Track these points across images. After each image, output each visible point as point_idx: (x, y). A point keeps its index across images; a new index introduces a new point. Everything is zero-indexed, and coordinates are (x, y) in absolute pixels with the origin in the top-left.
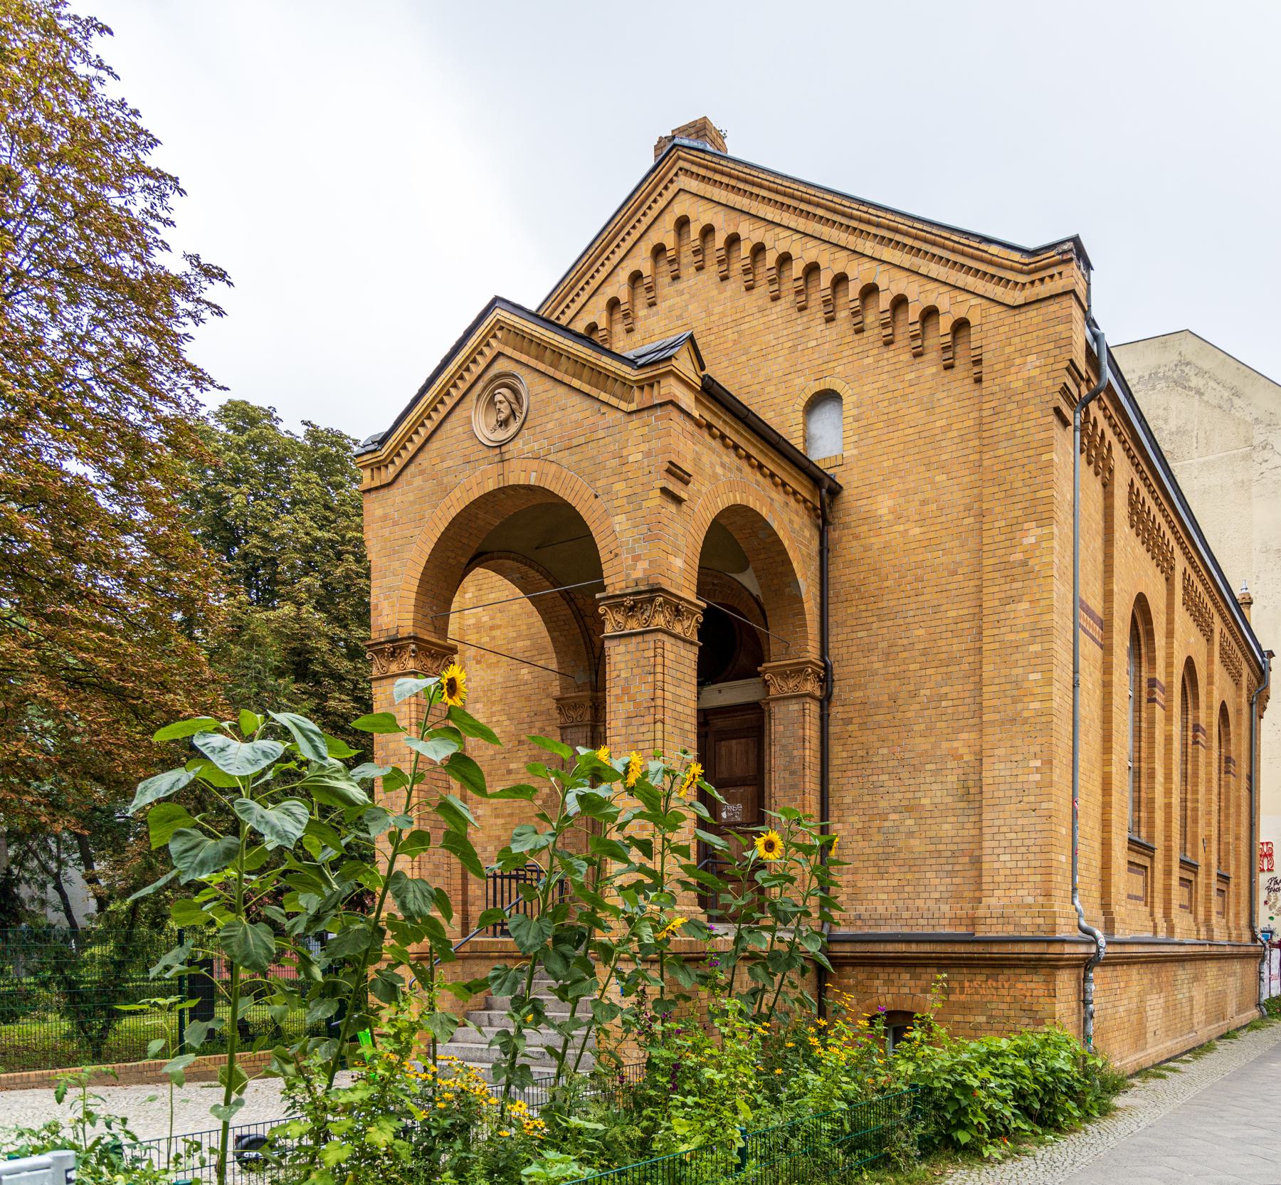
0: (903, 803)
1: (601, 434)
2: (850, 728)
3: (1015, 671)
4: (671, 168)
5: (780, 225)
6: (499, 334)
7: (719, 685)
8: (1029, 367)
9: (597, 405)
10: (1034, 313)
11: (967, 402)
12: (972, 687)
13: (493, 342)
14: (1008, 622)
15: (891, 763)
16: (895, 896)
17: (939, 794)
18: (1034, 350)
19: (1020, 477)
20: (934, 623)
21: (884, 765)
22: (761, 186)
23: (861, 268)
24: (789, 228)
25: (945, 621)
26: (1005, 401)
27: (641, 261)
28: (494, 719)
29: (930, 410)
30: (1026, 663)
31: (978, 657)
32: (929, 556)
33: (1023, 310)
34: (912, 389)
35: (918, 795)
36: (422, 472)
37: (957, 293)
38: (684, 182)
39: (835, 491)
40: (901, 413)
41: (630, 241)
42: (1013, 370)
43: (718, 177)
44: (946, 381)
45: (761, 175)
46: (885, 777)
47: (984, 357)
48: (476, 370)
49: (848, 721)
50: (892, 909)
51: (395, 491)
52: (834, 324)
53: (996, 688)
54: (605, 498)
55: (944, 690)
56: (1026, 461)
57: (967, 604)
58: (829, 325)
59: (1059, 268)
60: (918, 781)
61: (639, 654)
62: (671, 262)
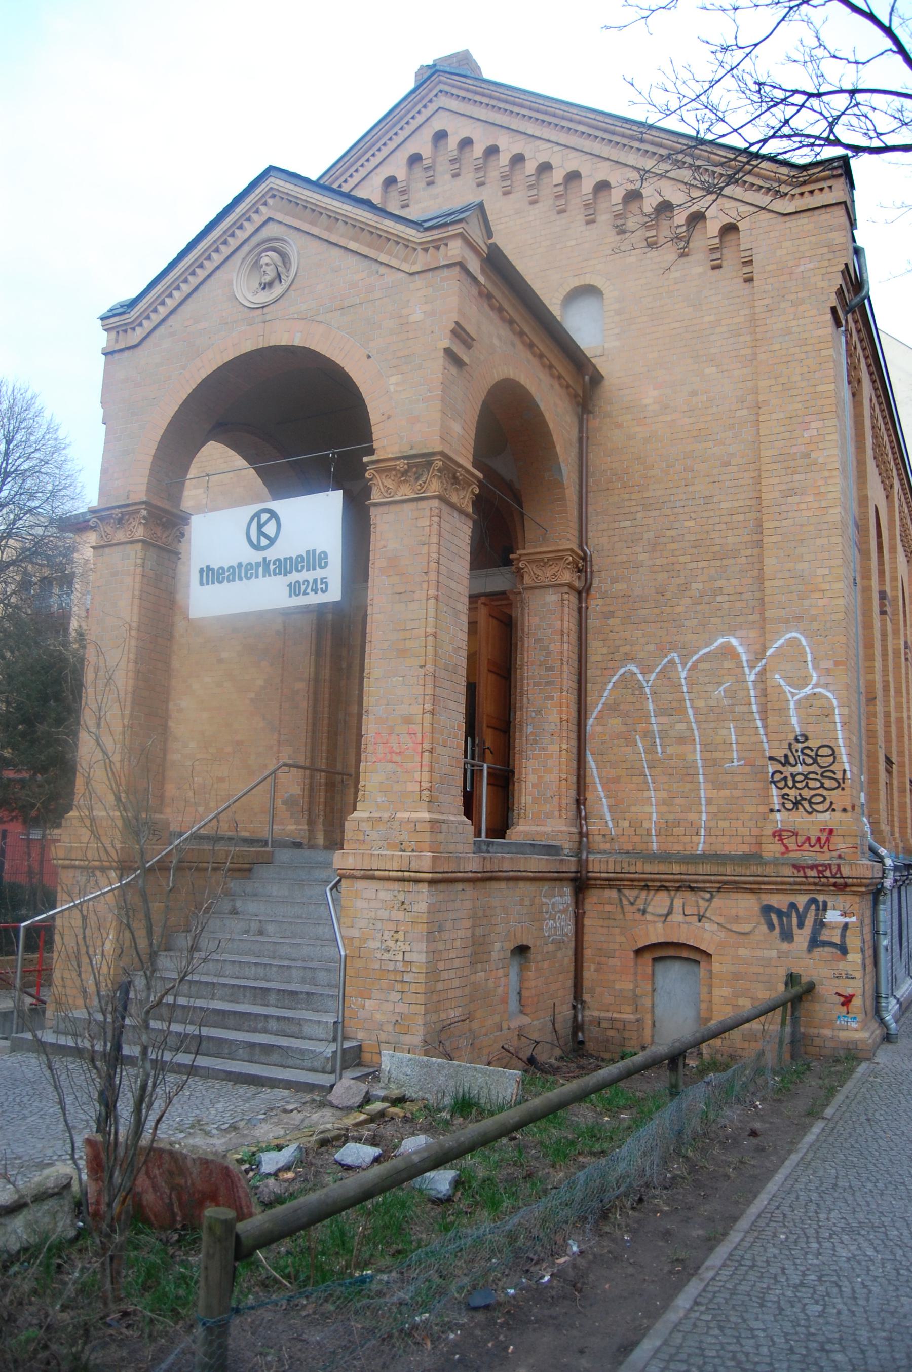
2: (611, 621)
5: (541, 139)
6: (271, 201)
9: (375, 266)
10: (806, 221)
12: (750, 581)
13: (263, 209)
14: (790, 515)
20: (705, 514)
22: (521, 106)
24: (549, 141)
27: (397, 168)
31: (756, 551)
38: (444, 101)
39: (597, 379)
41: (385, 151)
43: (478, 98)
45: (522, 96)
47: (754, 258)
48: (241, 235)
49: (610, 615)
51: (138, 351)
52: (594, 225)
56: (803, 356)
58: (589, 227)
59: (829, 183)
62: (427, 169)
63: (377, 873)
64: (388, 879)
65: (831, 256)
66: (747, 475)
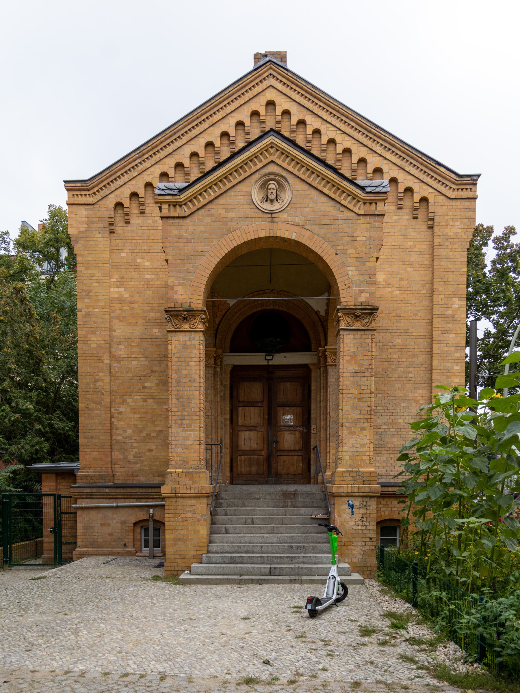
0: (389, 421)
1: (340, 222)
3: (448, 365)
4: (265, 72)
5: (330, 123)
7: (285, 354)
8: (456, 227)
10: (459, 204)
11: (423, 237)
14: (445, 342)
15: (383, 401)
16: (385, 465)
17: (407, 417)
18: (459, 220)
19: (452, 276)
20: (406, 337)
21: (380, 402)
23: (374, 158)
24: (335, 126)
25: (411, 337)
26: (445, 240)
28: (133, 356)
29: (405, 236)
30: (453, 361)
32: (404, 305)
33: (454, 201)
34: (396, 224)
35: (397, 417)
36: (211, 216)
37: (422, 184)
38: (272, 81)
40: (390, 234)
42: (449, 227)
44: (413, 224)
46: (380, 408)
47: (435, 217)
50: (384, 471)
51: (188, 221)
53: (439, 371)
54: (342, 256)
55: (411, 369)
56: (454, 270)
57: (422, 331)
60: (397, 411)
61: (362, 340)
63: (354, 494)
64: (358, 496)
65: (469, 224)
66: (424, 321)
